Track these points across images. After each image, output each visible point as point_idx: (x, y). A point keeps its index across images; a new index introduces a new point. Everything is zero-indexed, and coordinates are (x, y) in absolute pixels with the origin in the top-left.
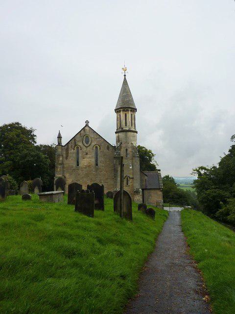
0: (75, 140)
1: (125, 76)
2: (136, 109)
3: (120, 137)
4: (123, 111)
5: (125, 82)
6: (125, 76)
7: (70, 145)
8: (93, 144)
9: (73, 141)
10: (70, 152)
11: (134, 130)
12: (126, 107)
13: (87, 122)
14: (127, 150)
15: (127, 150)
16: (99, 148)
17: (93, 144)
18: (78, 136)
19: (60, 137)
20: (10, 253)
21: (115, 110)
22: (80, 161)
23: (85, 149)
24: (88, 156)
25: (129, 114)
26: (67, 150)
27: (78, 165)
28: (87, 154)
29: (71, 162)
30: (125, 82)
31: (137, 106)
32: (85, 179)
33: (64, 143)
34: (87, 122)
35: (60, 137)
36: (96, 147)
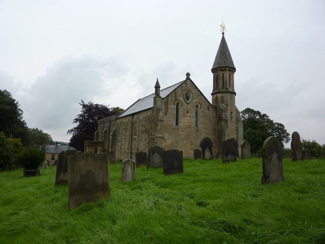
0: (176, 93)
1: (223, 33)
2: (235, 69)
3: (225, 99)
4: (229, 70)
5: (223, 40)
6: (223, 33)
7: (170, 99)
8: (194, 101)
9: (173, 95)
10: (169, 106)
11: (231, 90)
12: (82, 101)
13: (188, 75)
14: (231, 112)
15: (231, 112)
16: (200, 106)
17: (194, 101)
18: (179, 89)
19: (157, 86)
20: (135, 162)
21: (212, 70)
22: (180, 118)
23: (186, 106)
24: (189, 114)
25: (227, 73)
26: (167, 103)
27: (177, 124)
28: (188, 112)
29: (170, 120)
30: (223, 40)
31: (236, 66)
32: (185, 142)
33: (163, 95)
34: (188, 75)
35: (157, 86)
36: (197, 106)
